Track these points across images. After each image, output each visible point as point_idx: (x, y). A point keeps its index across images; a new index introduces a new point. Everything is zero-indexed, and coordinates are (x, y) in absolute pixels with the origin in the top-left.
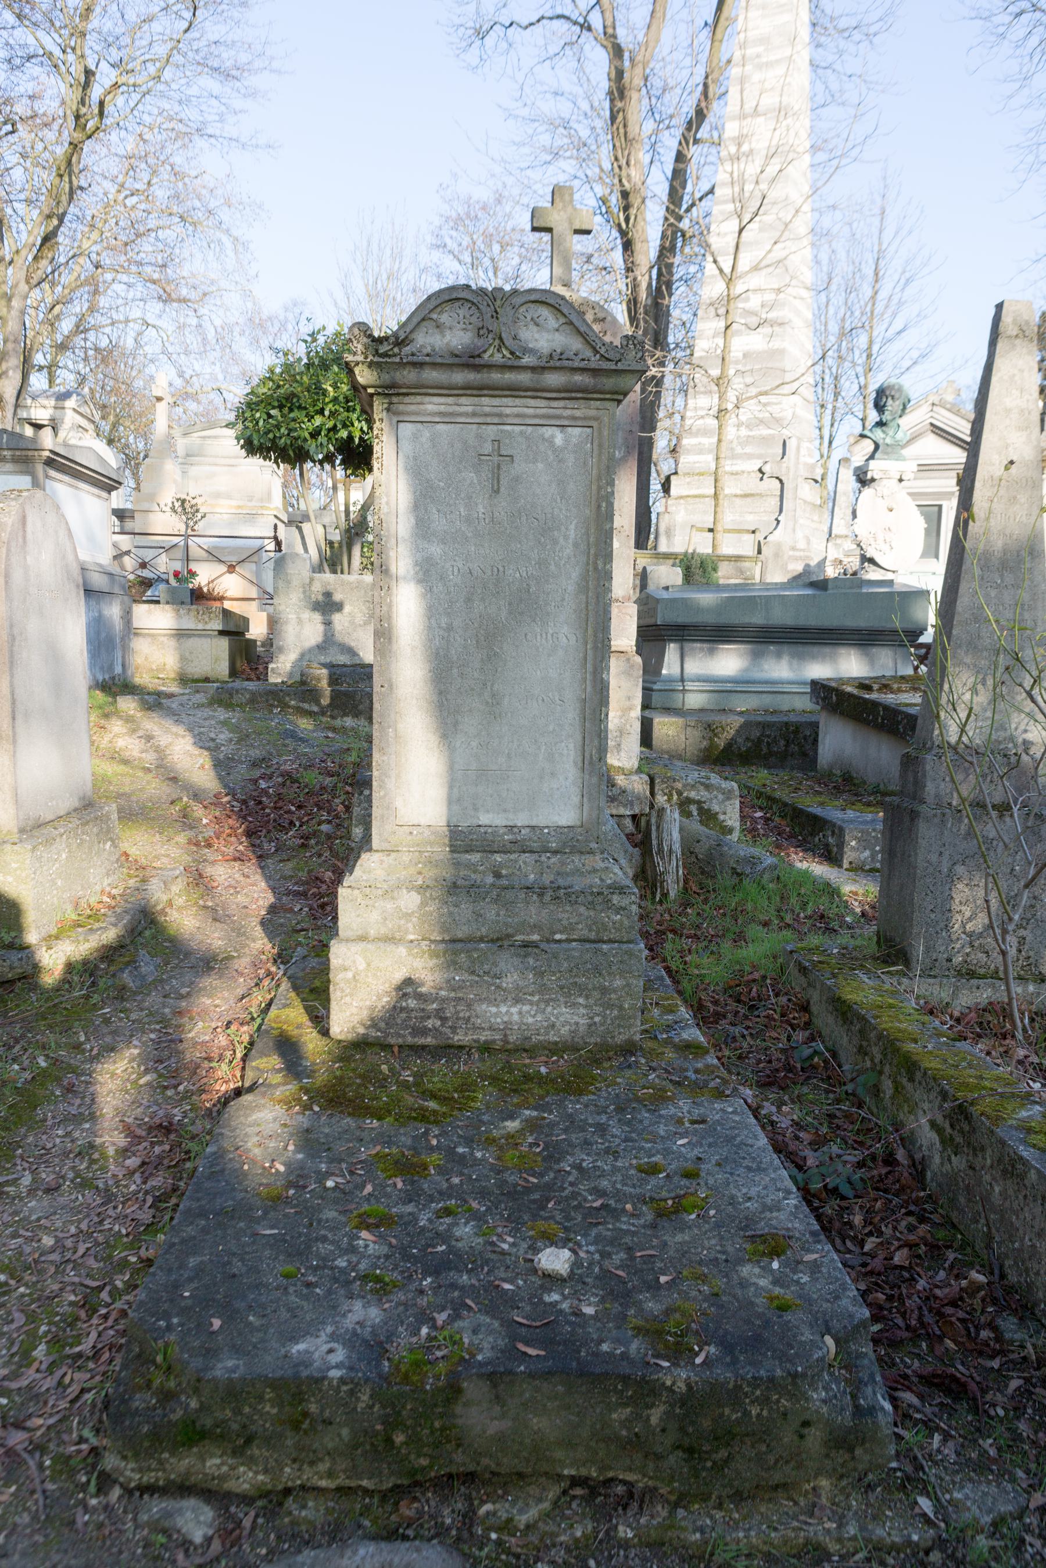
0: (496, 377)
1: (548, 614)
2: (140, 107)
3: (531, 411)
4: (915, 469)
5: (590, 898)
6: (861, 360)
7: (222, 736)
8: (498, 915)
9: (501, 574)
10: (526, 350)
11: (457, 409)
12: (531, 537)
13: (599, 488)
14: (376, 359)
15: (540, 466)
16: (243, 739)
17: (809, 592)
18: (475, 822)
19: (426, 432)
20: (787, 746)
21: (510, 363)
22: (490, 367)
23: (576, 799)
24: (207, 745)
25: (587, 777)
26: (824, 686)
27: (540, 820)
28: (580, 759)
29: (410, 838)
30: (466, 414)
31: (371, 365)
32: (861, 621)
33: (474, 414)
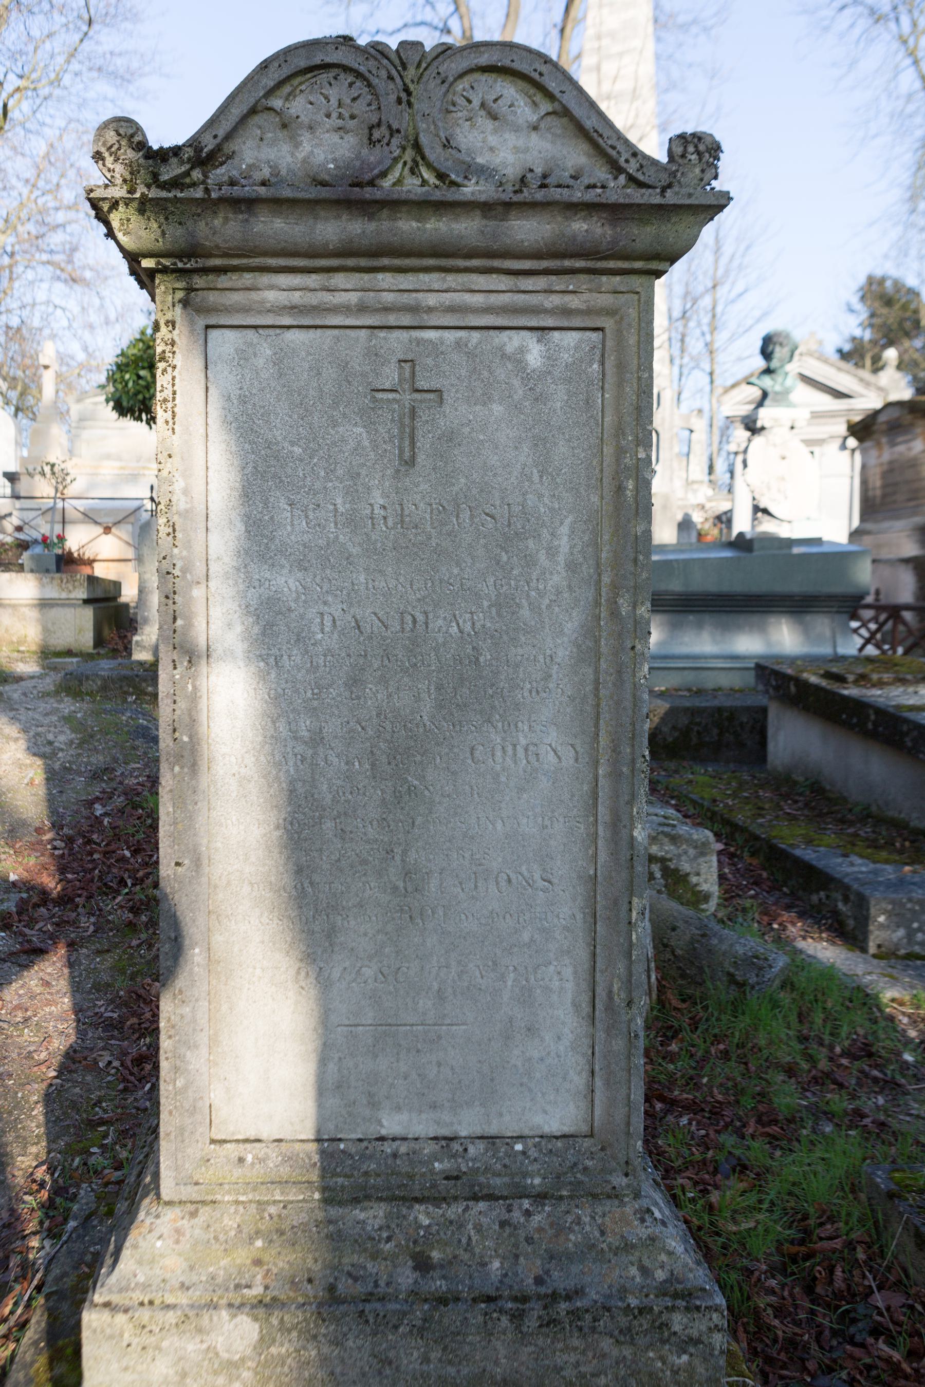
0: (408, 227)
1: (517, 706)
2: (42, 109)
3: (477, 300)
4: (808, 416)
5: (623, 1321)
6: (706, 320)
7: (62, 738)
8: (426, 1360)
9: (420, 628)
10: (470, 170)
11: (327, 297)
12: (481, 552)
13: (620, 452)
14: (154, 193)
15: (497, 409)
16: (86, 740)
17: (728, 554)
18: (373, 1131)
19: (265, 347)
20: (721, 734)
21: (437, 195)
22: (394, 205)
23: (579, 1081)
24: (43, 749)
25: (601, 1035)
26: (777, 674)
27: (506, 1125)
28: (585, 998)
29: (238, 1172)
30: (346, 309)
31: (144, 206)
32: (795, 586)
33: (362, 309)
